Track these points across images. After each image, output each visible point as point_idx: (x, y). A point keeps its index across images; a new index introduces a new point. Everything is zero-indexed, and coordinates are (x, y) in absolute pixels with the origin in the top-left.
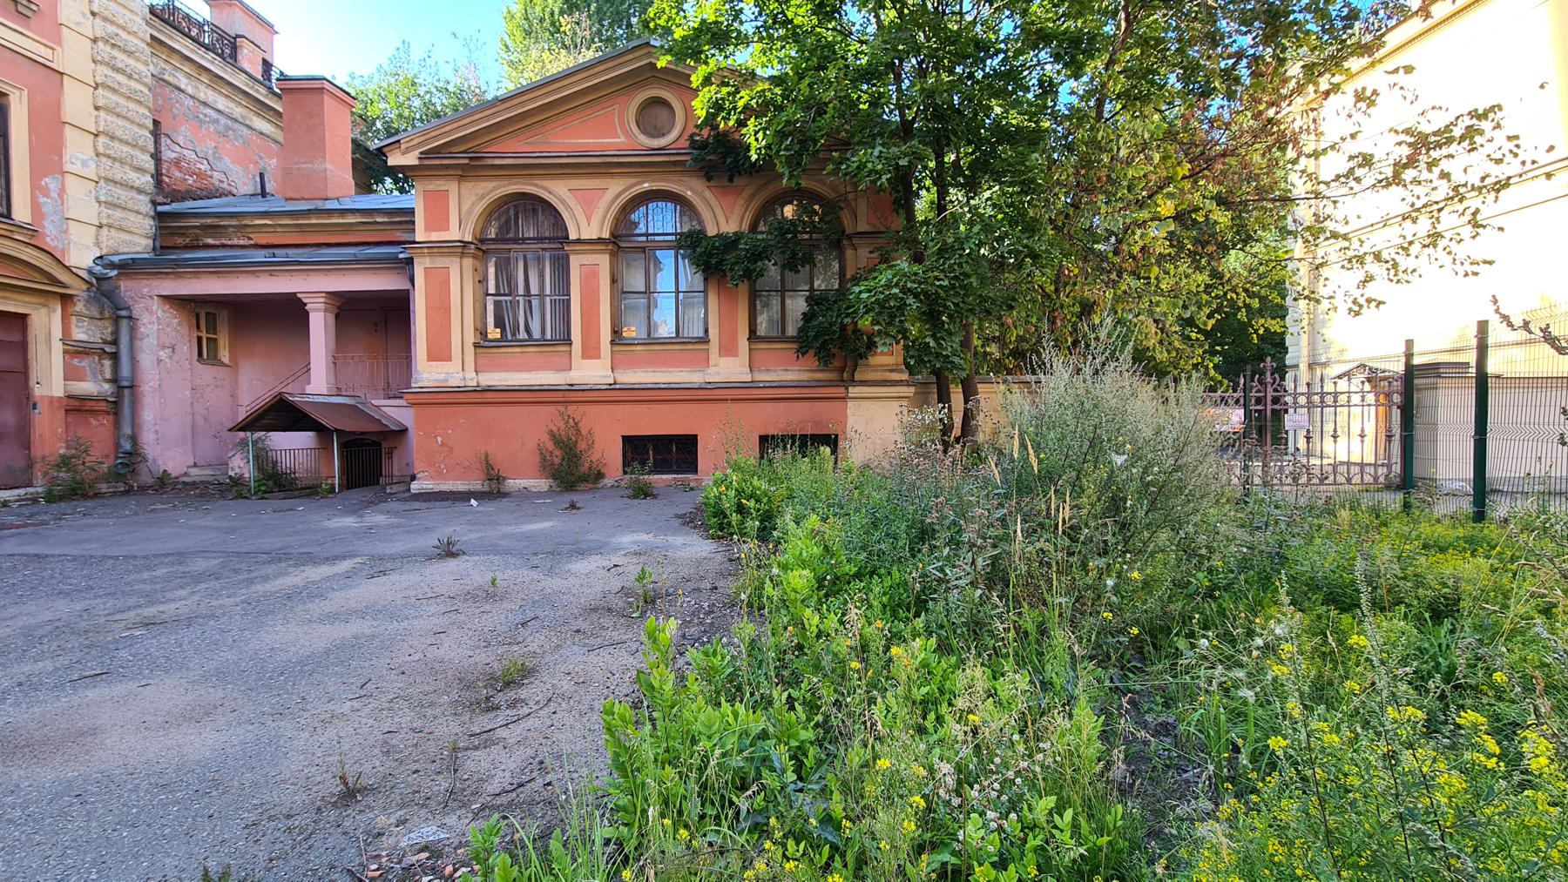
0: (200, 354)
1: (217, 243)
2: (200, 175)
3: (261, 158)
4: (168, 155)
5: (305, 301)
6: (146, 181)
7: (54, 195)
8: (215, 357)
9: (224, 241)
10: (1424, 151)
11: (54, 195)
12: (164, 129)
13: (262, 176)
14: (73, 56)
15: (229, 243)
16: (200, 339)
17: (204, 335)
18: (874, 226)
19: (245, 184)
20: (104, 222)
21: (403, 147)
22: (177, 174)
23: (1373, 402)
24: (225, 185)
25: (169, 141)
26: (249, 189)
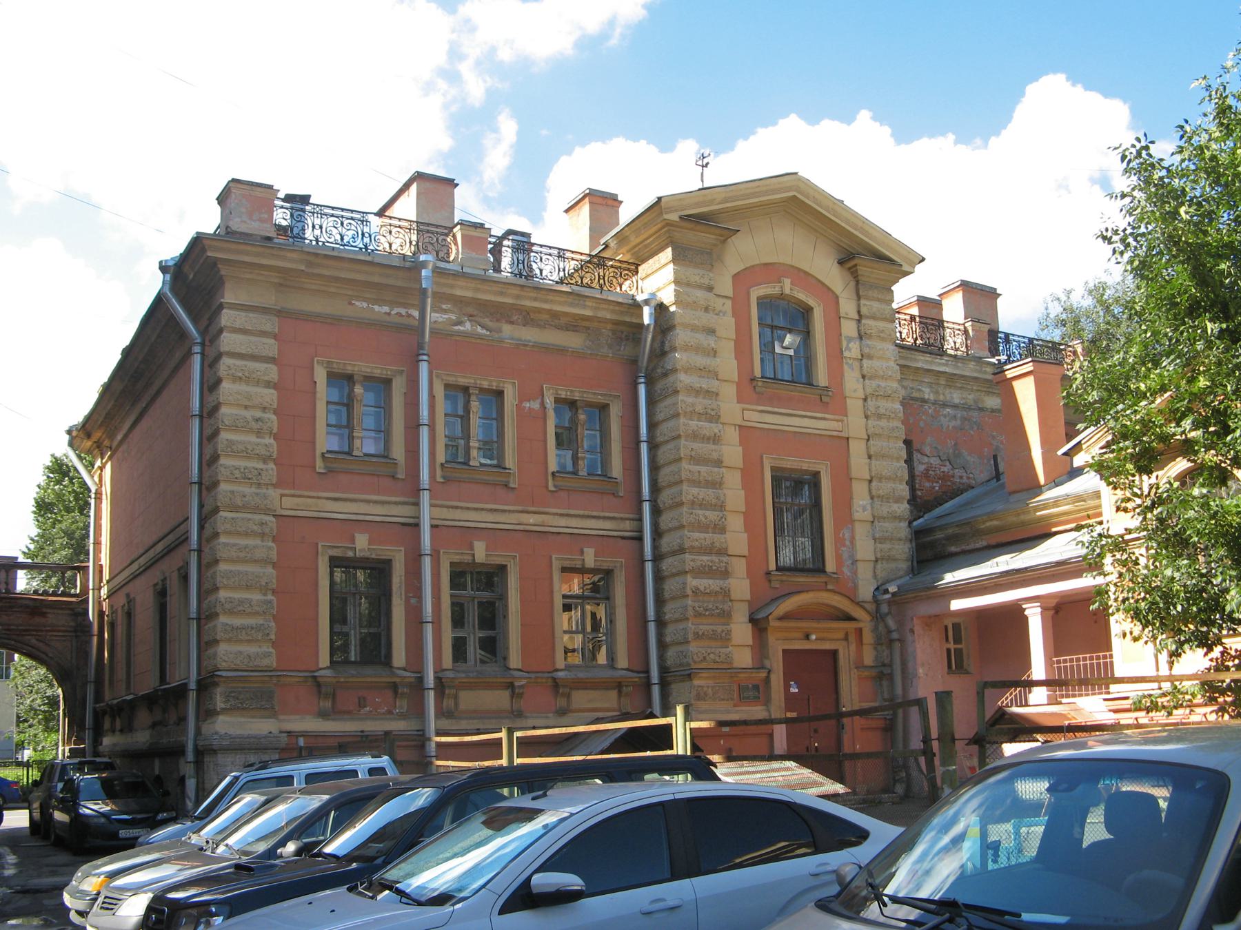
0: (950, 666)
1: (958, 550)
2: (945, 477)
3: (994, 437)
4: (919, 469)
5: (1024, 606)
6: (904, 489)
7: (848, 543)
8: (962, 667)
9: (964, 547)
10: (1171, 608)
11: (848, 543)
12: (916, 445)
13: (995, 458)
14: (855, 424)
15: (968, 548)
16: (949, 651)
17: (952, 646)
18: (400, 869)
19: (981, 472)
20: (879, 556)
21: (1084, 446)
22: (927, 484)
23: (1164, 689)
24: (965, 480)
25: (919, 456)
26: (984, 476)
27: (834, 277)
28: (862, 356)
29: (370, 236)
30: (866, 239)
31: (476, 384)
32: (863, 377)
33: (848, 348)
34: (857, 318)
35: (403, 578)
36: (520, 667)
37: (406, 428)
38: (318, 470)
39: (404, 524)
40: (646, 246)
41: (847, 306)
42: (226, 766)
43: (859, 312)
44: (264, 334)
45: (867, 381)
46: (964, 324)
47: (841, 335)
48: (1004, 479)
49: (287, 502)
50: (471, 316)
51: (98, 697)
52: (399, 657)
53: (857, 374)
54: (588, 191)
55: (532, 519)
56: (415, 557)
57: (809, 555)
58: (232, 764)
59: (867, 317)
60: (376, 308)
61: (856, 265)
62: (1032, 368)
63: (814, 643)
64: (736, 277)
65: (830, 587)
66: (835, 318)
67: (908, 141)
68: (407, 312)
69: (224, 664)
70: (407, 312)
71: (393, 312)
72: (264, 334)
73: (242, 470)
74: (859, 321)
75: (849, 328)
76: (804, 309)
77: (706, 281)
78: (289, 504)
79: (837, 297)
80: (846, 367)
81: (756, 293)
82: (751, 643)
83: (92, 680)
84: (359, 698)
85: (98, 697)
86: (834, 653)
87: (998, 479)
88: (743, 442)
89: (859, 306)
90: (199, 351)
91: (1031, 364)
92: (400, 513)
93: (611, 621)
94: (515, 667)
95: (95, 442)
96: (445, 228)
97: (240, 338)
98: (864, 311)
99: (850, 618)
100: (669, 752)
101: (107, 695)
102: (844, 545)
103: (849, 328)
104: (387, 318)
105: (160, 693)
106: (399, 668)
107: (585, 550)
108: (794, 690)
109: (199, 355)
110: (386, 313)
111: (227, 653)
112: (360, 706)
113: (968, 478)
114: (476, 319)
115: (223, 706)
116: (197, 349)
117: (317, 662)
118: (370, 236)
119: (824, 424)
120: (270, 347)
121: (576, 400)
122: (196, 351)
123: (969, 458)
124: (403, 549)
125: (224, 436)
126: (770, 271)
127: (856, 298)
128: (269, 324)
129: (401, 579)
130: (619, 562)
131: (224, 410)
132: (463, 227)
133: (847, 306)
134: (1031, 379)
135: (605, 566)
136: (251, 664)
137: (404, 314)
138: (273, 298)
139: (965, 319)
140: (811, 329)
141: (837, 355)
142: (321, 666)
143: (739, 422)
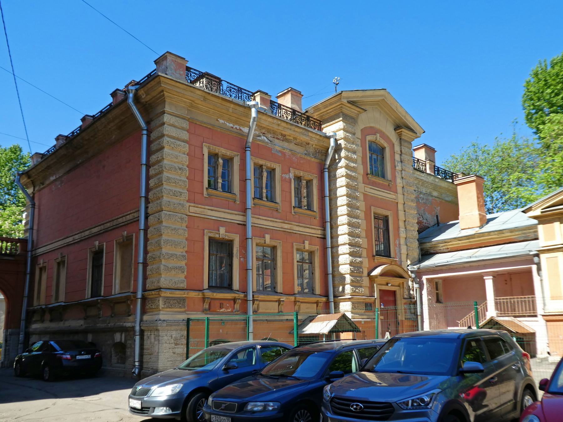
7: (398, 246)
27: (393, 136)
28: (402, 169)
29: (223, 91)
30: (405, 120)
31: (265, 164)
32: (402, 178)
33: (398, 166)
34: (400, 153)
35: (238, 248)
36: (282, 292)
37: (240, 180)
38: (205, 196)
39: (238, 224)
40: (328, 113)
41: (397, 148)
42: (163, 337)
43: (401, 151)
44: (183, 129)
45: (404, 180)
46: (425, 161)
47: (395, 160)
48: (440, 225)
49: (192, 209)
50: (264, 134)
51: (30, 303)
52: (236, 285)
53: (400, 176)
54: (290, 89)
55: (286, 226)
56: (244, 240)
57: (383, 249)
58: (166, 335)
59: (404, 154)
60: (228, 124)
61: (401, 131)
62: (475, 179)
63: (389, 288)
64: (362, 130)
65: (393, 264)
66: (393, 153)
67: (56, 140)
68: (239, 128)
69: (164, 285)
70: (239, 128)
71: (234, 127)
72: (183, 129)
73: (174, 192)
74: (401, 155)
75: (397, 157)
76: (382, 147)
77: (353, 130)
78: (194, 210)
79: (393, 145)
80: (397, 173)
81: (369, 138)
82: (369, 286)
83: (26, 296)
84: (220, 304)
85: (30, 303)
86: (394, 293)
87: (438, 225)
88: (365, 200)
89: (401, 148)
90: (146, 133)
91: (475, 177)
92: (238, 218)
93: (312, 274)
94: (280, 292)
95: (32, 181)
96: (252, 93)
97: (174, 129)
98: (403, 151)
99: (401, 277)
100: (417, 332)
101: (35, 303)
102: (396, 247)
103: (397, 157)
104: (231, 129)
105: (99, 301)
106: (236, 290)
107: (306, 241)
108: (382, 307)
109: (146, 135)
110: (231, 127)
111: (165, 280)
112: (220, 308)
113: (428, 224)
114: (266, 135)
115: (163, 306)
116: (145, 132)
117: (203, 287)
118: (223, 91)
119: (390, 196)
120: (185, 135)
121: (301, 176)
122: (144, 133)
123: (428, 215)
124: (238, 235)
125: (165, 174)
126: (373, 131)
127: (399, 145)
128: (186, 125)
129: (237, 249)
130: (316, 248)
131: (165, 162)
132: (261, 93)
133: (397, 148)
134: (474, 184)
135: (312, 250)
136: (176, 286)
137: (238, 128)
138: (186, 112)
139: (426, 159)
140: (385, 156)
141: (394, 167)
142: (205, 288)
143: (363, 192)
